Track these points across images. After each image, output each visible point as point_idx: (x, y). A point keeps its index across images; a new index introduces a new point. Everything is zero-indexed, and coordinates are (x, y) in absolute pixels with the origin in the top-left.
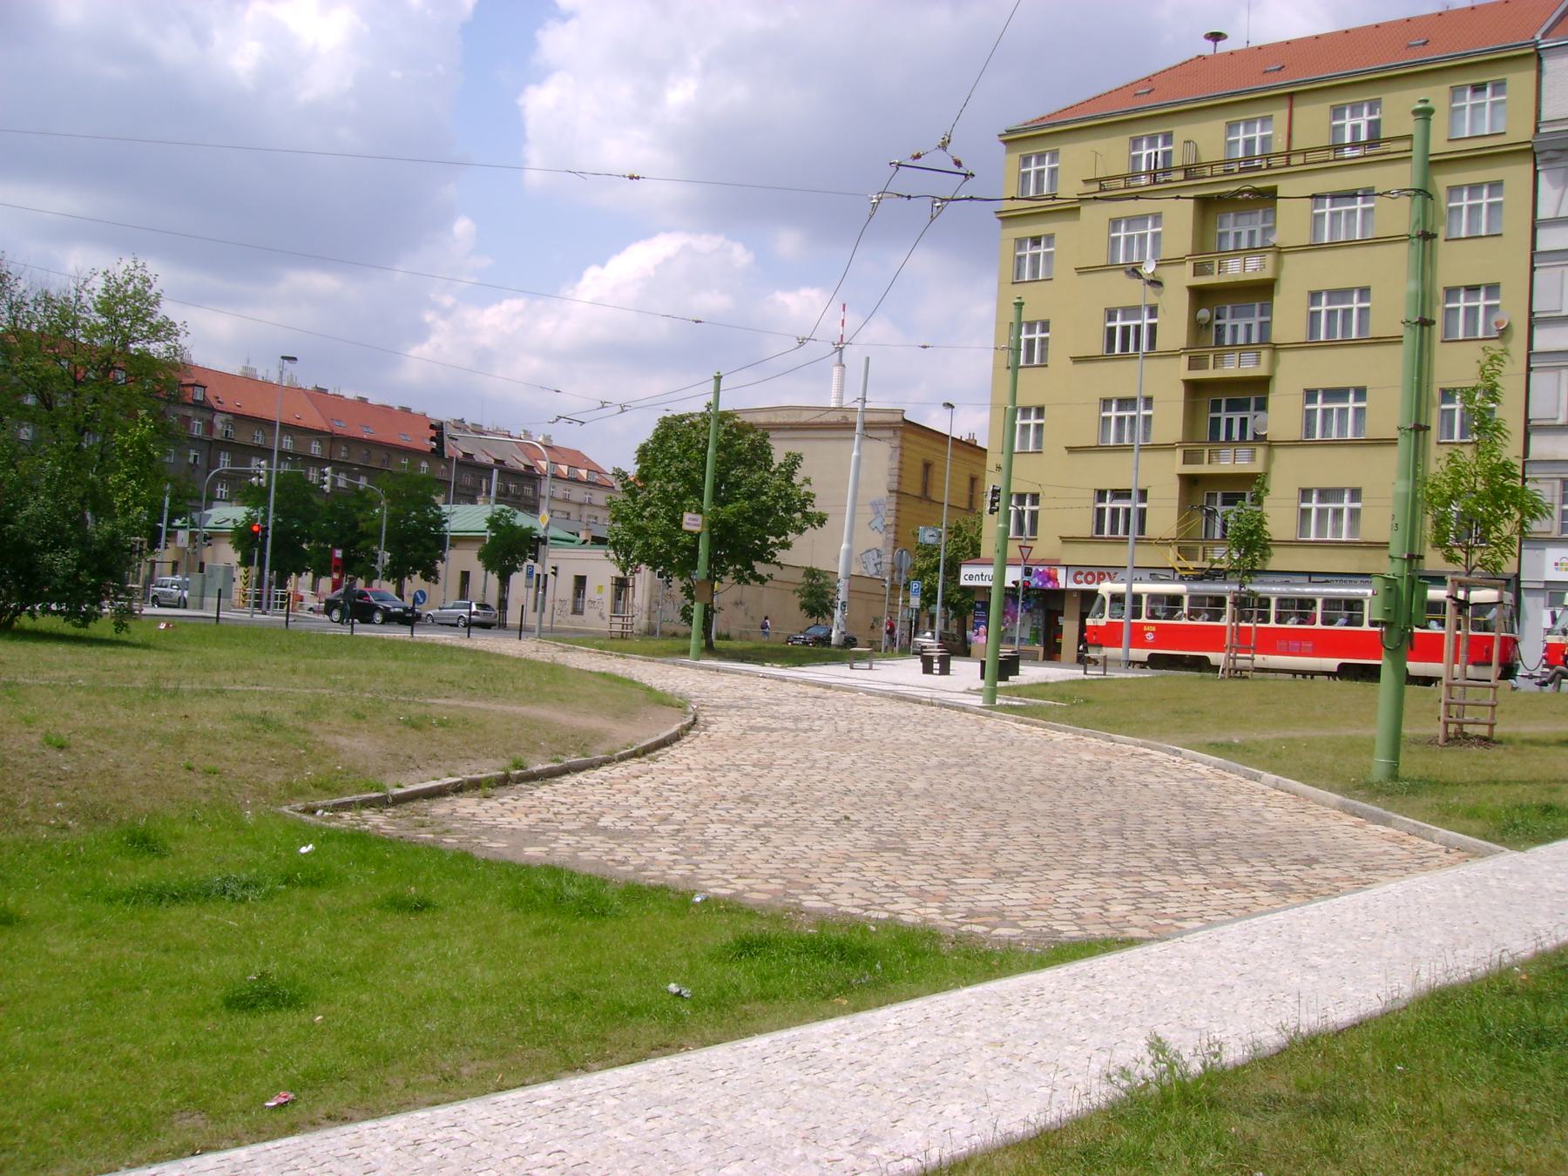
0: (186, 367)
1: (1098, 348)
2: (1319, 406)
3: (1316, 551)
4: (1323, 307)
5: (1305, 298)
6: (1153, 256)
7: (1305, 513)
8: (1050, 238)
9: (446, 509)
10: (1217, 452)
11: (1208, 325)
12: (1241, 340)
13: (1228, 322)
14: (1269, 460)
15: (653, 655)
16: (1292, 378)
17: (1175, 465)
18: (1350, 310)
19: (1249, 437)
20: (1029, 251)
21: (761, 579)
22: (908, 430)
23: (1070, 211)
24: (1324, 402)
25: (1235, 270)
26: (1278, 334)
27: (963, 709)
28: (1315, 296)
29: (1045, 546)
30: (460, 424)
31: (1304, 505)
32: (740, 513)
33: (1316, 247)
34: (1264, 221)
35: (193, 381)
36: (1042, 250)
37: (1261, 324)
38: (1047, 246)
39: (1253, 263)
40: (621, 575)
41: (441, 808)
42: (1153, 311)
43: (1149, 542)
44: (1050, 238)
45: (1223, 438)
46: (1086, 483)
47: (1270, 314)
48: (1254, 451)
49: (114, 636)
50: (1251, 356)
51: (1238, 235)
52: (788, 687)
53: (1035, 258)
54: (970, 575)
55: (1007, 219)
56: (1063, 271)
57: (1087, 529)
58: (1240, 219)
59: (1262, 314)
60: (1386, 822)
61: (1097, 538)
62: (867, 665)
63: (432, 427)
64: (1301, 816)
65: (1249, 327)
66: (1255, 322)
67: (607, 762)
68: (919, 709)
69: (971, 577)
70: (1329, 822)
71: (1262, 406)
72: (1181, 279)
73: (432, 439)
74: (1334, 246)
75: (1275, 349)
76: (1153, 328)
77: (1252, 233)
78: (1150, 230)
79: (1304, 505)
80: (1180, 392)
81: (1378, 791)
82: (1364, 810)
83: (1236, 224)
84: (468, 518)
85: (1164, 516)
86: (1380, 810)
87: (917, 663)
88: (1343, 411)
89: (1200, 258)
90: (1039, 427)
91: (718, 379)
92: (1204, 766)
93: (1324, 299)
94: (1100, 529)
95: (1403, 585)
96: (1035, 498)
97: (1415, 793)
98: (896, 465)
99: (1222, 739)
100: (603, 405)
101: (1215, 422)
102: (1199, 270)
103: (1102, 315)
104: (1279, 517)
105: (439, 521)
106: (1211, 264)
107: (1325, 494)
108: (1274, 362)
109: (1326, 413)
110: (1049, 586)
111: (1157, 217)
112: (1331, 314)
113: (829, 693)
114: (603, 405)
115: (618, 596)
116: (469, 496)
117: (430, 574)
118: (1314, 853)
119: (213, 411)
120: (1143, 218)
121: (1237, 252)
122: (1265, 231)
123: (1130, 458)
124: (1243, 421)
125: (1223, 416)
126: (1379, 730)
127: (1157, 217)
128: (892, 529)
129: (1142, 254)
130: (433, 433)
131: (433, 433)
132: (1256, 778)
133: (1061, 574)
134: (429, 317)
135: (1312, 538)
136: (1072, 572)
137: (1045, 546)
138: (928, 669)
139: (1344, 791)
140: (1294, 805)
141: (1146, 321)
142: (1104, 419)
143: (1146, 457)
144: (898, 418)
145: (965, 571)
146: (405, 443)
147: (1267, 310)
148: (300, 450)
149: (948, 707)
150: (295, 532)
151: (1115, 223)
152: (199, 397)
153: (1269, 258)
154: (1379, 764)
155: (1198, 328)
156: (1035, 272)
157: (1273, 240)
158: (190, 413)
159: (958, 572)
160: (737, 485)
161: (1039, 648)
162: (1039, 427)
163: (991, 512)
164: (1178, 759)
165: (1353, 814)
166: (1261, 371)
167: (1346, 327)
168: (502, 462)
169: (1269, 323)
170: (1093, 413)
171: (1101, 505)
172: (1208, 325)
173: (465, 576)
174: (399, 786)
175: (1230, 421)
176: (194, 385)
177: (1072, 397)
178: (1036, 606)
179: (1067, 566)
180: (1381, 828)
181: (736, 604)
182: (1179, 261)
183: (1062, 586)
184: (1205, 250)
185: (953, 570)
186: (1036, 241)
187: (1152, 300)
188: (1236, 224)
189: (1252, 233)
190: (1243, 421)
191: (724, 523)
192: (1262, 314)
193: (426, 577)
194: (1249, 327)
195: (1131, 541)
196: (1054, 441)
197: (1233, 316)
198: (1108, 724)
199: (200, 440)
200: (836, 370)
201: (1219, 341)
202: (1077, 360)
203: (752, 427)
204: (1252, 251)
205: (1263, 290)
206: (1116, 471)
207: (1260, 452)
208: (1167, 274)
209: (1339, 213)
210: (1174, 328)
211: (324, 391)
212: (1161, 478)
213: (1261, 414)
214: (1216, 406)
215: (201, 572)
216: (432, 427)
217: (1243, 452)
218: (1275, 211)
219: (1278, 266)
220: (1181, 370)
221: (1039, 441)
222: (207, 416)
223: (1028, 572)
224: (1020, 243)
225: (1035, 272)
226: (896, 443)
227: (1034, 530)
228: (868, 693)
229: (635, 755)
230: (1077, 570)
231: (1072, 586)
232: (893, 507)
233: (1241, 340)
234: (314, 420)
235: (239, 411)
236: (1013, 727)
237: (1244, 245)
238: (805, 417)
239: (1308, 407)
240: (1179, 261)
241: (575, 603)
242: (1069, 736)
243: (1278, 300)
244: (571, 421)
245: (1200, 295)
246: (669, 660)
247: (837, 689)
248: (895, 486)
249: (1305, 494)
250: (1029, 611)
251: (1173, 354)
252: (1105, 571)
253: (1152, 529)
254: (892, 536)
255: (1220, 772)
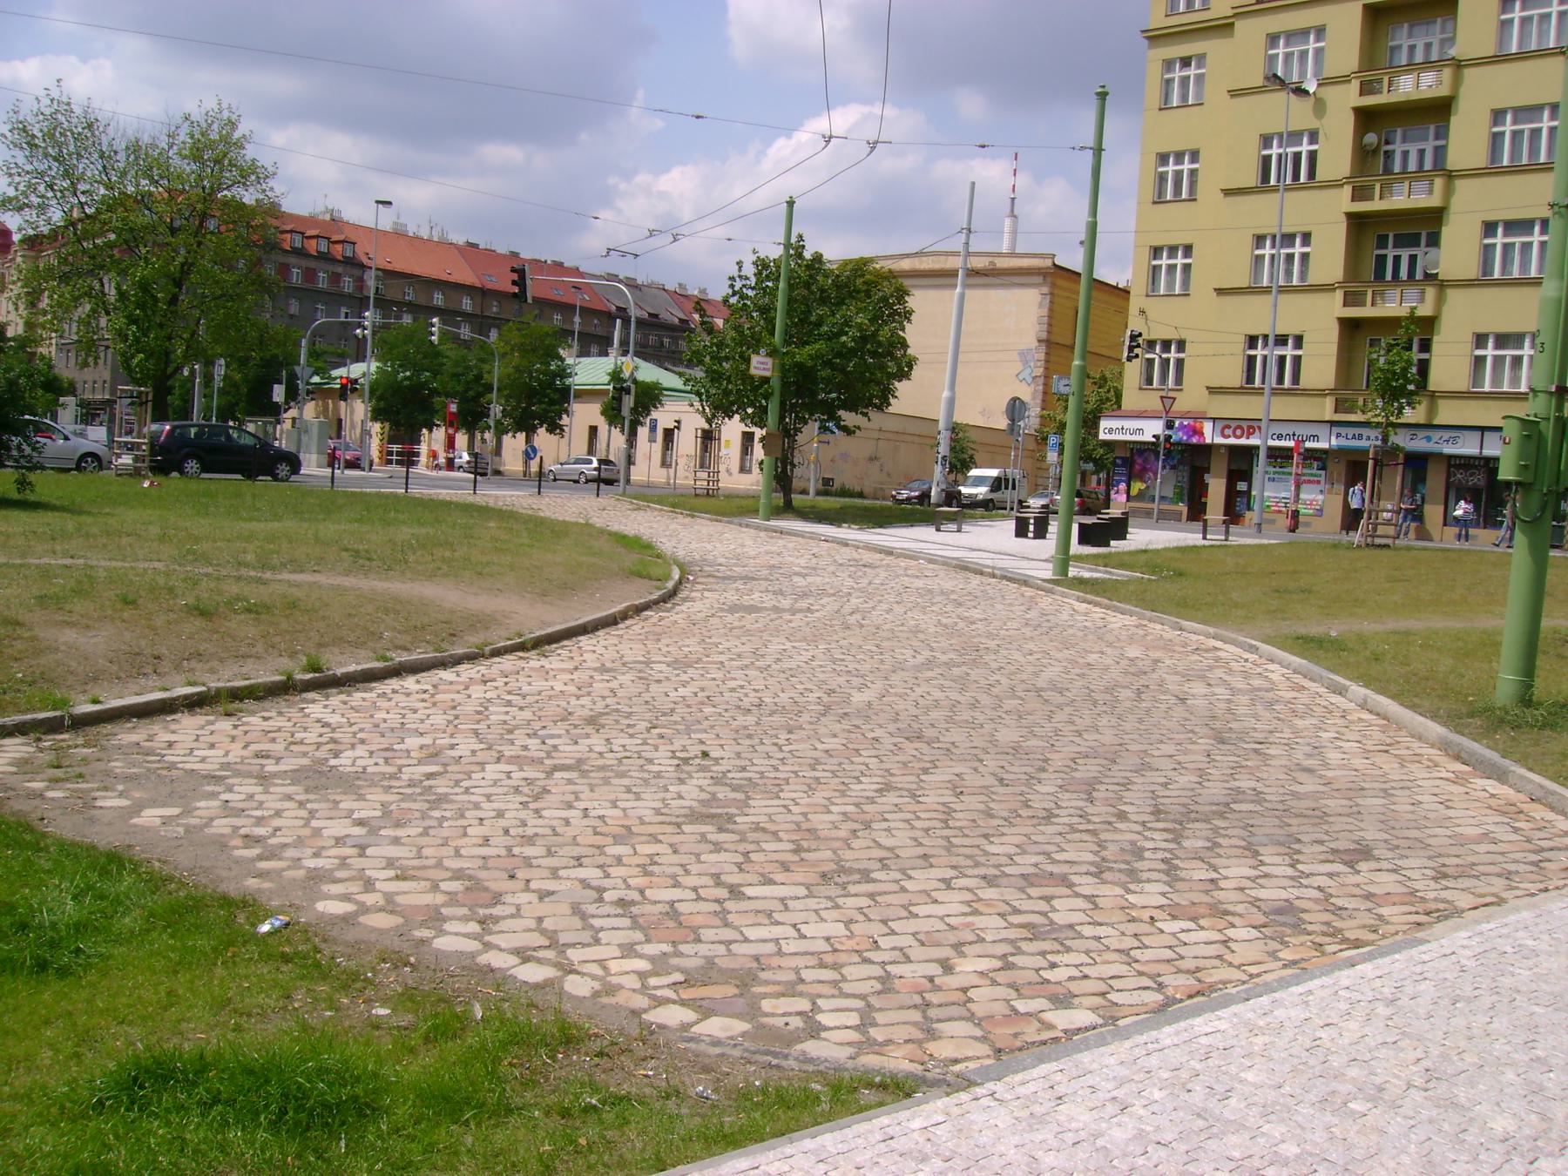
0: (273, 210)
1: (1251, 178)
2: (1499, 240)
3: (1491, 403)
4: (1508, 127)
5: (1487, 117)
6: (1316, 74)
7: (1479, 361)
8: (1201, 58)
9: (569, 361)
10: (1382, 293)
11: (1375, 151)
12: (1412, 166)
13: (1398, 148)
14: (1440, 301)
15: (723, 514)
16: (1470, 206)
17: (1334, 307)
18: (1531, 244)
19: (1419, 275)
20: (1177, 74)
21: (848, 431)
22: (1057, 277)
23: (1223, 28)
24: (1505, 235)
25: (1408, 88)
26: (1454, 161)
27: (1025, 582)
28: (1498, 116)
29: (1191, 398)
30: (538, 264)
31: (1479, 352)
32: (818, 356)
33: (1501, 58)
34: (1443, 31)
35: (342, 237)
36: (1192, 72)
37: (1436, 149)
38: (1198, 67)
39: (1428, 78)
40: (707, 426)
41: (159, 732)
42: (1314, 137)
43: (1306, 393)
44: (1201, 58)
45: (1389, 277)
46: (1240, 325)
47: (1446, 137)
48: (1423, 292)
49: (16, 496)
50: (1424, 185)
51: (1412, 48)
52: (847, 553)
53: (1185, 81)
54: (1110, 429)
55: (1156, 38)
56: (1215, 92)
57: (1236, 378)
58: (1416, 30)
59: (1437, 138)
60: (1501, 776)
61: (1248, 386)
62: (954, 527)
63: (513, 270)
64: (1379, 759)
65: (1422, 152)
66: (1429, 145)
67: (471, 658)
68: (976, 580)
69: (1111, 431)
70: (1418, 771)
71: (1434, 241)
72: (1349, 97)
73: (514, 283)
74: (1522, 56)
75: (1450, 176)
76: (1313, 156)
77: (1428, 46)
78: (1312, 45)
79: (1479, 352)
80: (1340, 230)
81: (1502, 721)
82: (1472, 753)
83: (1410, 36)
84: (591, 371)
85: (1320, 366)
86: (1494, 756)
87: (1011, 525)
88: (1527, 247)
89: (1369, 76)
90: (1187, 268)
91: (791, 204)
92: (1279, 669)
93: (1509, 117)
94: (1250, 378)
95: (1549, 430)
96: (1181, 345)
97: (1552, 727)
98: (1045, 312)
99: (1315, 630)
100: (652, 233)
101: (1381, 260)
102: (1366, 89)
103: (1256, 141)
104: (1448, 364)
105: (563, 373)
106: (1380, 81)
107: (1503, 340)
108: (1448, 192)
109: (1507, 248)
110: (1194, 440)
111: (1320, 31)
112: (1516, 135)
113: (888, 560)
114: (652, 233)
115: (705, 449)
116: (595, 343)
117: (555, 428)
118: (1371, 834)
119: (363, 267)
120: (1303, 33)
121: (1411, 67)
122: (1443, 42)
123: (1267, 300)
124: (1413, 259)
125: (1390, 253)
126: (1508, 623)
127: (1320, 31)
128: (1041, 381)
129: (1303, 73)
130: (515, 277)
131: (515, 277)
132: (1340, 691)
133: (1208, 428)
134: (612, 181)
135: (1487, 389)
136: (1220, 425)
137: (1191, 398)
138: (1021, 531)
139: (1453, 720)
140: (1377, 735)
141: (1305, 148)
142: (1257, 257)
143: (1283, 298)
144: (1048, 263)
145: (1104, 424)
146: (558, 298)
147: (1442, 133)
148: (451, 306)
149: (1009, 579)
150: (424, 386)
151: (1273, 39)
152: (349, 254)
153: (1447, 73)
154: (1506, 681)
155: (1364, 156)
156: (1184, 97)
157: (1452, 52)
158: (340, 270)
159: (1096, 426)
160: (819, 324)
161: (1183, 508)
162: (1187, 268)
163: (1129, 359)
164: (1252, 657)
165: (1457, 758)
166: (1434, 201)
167: (1534, 150)
168: (656, 316)
169: (1444, 147)
170: (1245, 249)
171: (1252, 352)
172: (1375, 151)
173: (593, 430)
174: (96, 702)
175: (1397, 259)
176: (342, 242)
177: (1222, 235)
178: (1181, 462)
179: (1214, 419)
180: (1492, 786)
181: (871, 459)
182: (1344, 80)
183: (1208, 441)
184: (1375, 60)
185: (1090, 422)
186: (1186, 62)
187: (1312, 124)
188: (1410, 36)
189: (1428, 46)
190: (1413, 259)
191: (800, 366)
192: (1437, 138)
193: (551, 431)
194: (1422, 152)
195: (1267, 391)
196: (1203, 282)
197: (1404, 141)
198: (1183, 607)
199: (350, 296)
200: (1008, 222)
201: (1388, 170)
202: (1228, 192)
203: (892, 275)
204: (1428, 65)
205: (1438, 111)
206: (1257, 315)
207: (1430, 292)
208: (1330, 93)
209: (1530, 18)
210: (1337, 157)
211: (475, 246)
212: (1318, 322)
213: (1432, 250)
214: (1382, 242)
215: (329, 422)
216: (513, 270)
217: (1412, 292)
218: (1455, 19)
219: (1457, 82)
220: (1343, 201)
221: (1186, 282)
222: (357, 272)
223: (1169, 425)
224: (1168, 65)
225: (1184, 97)
226: (1045, 290)
227: (1179, 380)
228: (930, 561)
229: (522, 647)
230: (1224, 423)
231: (1219, 440)
232: (1042, 356)
233: (1412, 166)
234: (466, 276)
235: (389, 267)
236: (1075, 610)
237: (1419, 58)
238: (1016, 280)
239: (1487, 241)
240: (1344, 80)
241: (742, 460)
242: (1133, 621)
243: (1455, 121)
244: (624, 254)
245: (1366, 118)
246: (736, 520)
247: (899, 556)
248: (1044, 335)
249: (1480, 340)
250: (1173, 467)
251: (1335, 185)
252: (1255, 424)
253: (1308, 379)
254: (1041, 388)
255: (1298, 679)
